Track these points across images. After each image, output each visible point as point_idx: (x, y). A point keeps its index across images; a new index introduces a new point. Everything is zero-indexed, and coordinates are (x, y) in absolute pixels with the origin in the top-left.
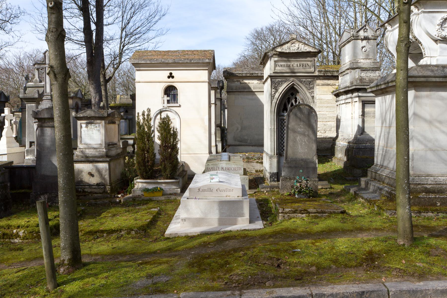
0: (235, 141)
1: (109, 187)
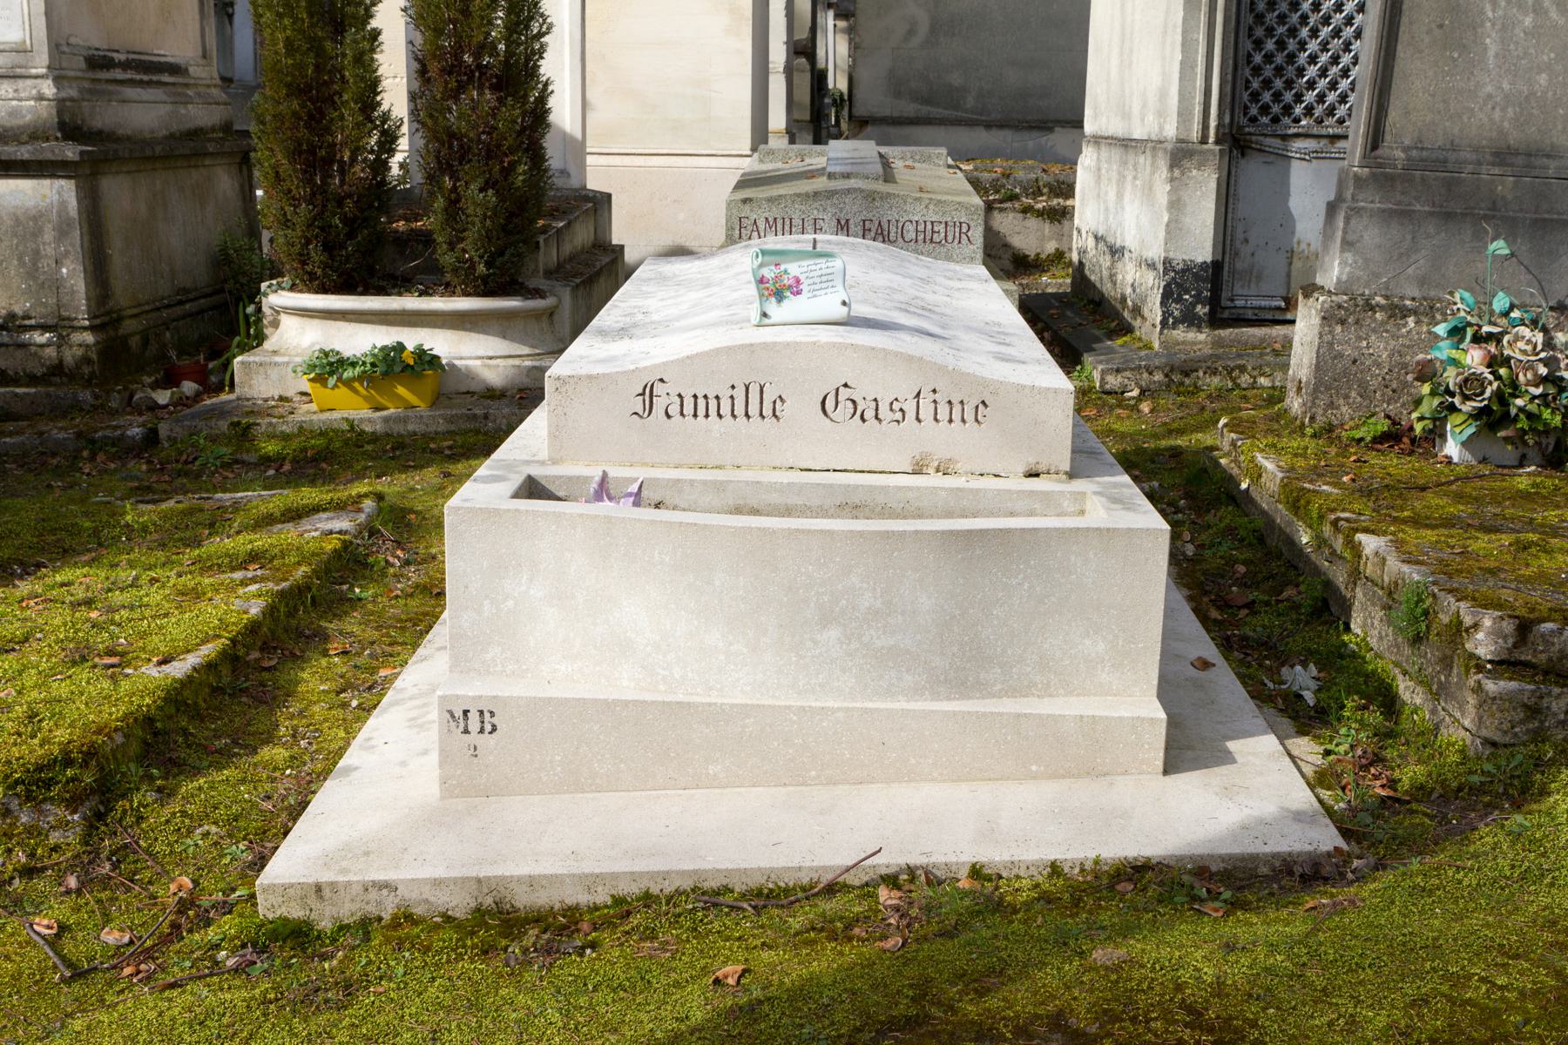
0: (898, 94)
1: (89, 338)
